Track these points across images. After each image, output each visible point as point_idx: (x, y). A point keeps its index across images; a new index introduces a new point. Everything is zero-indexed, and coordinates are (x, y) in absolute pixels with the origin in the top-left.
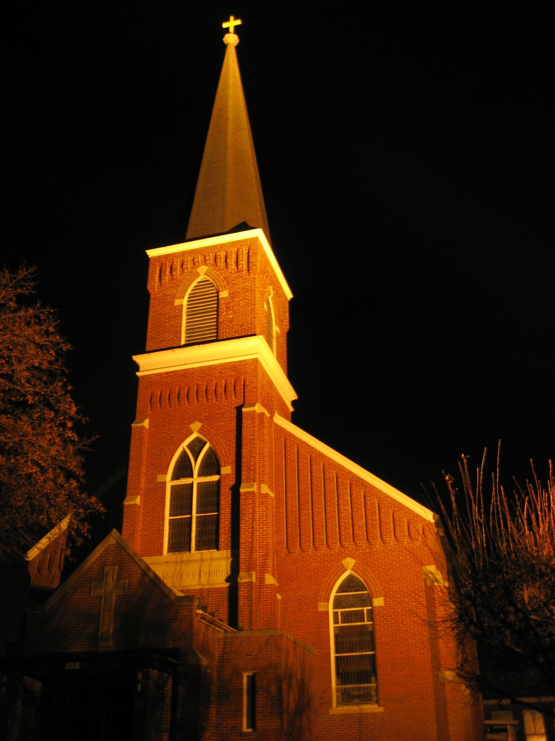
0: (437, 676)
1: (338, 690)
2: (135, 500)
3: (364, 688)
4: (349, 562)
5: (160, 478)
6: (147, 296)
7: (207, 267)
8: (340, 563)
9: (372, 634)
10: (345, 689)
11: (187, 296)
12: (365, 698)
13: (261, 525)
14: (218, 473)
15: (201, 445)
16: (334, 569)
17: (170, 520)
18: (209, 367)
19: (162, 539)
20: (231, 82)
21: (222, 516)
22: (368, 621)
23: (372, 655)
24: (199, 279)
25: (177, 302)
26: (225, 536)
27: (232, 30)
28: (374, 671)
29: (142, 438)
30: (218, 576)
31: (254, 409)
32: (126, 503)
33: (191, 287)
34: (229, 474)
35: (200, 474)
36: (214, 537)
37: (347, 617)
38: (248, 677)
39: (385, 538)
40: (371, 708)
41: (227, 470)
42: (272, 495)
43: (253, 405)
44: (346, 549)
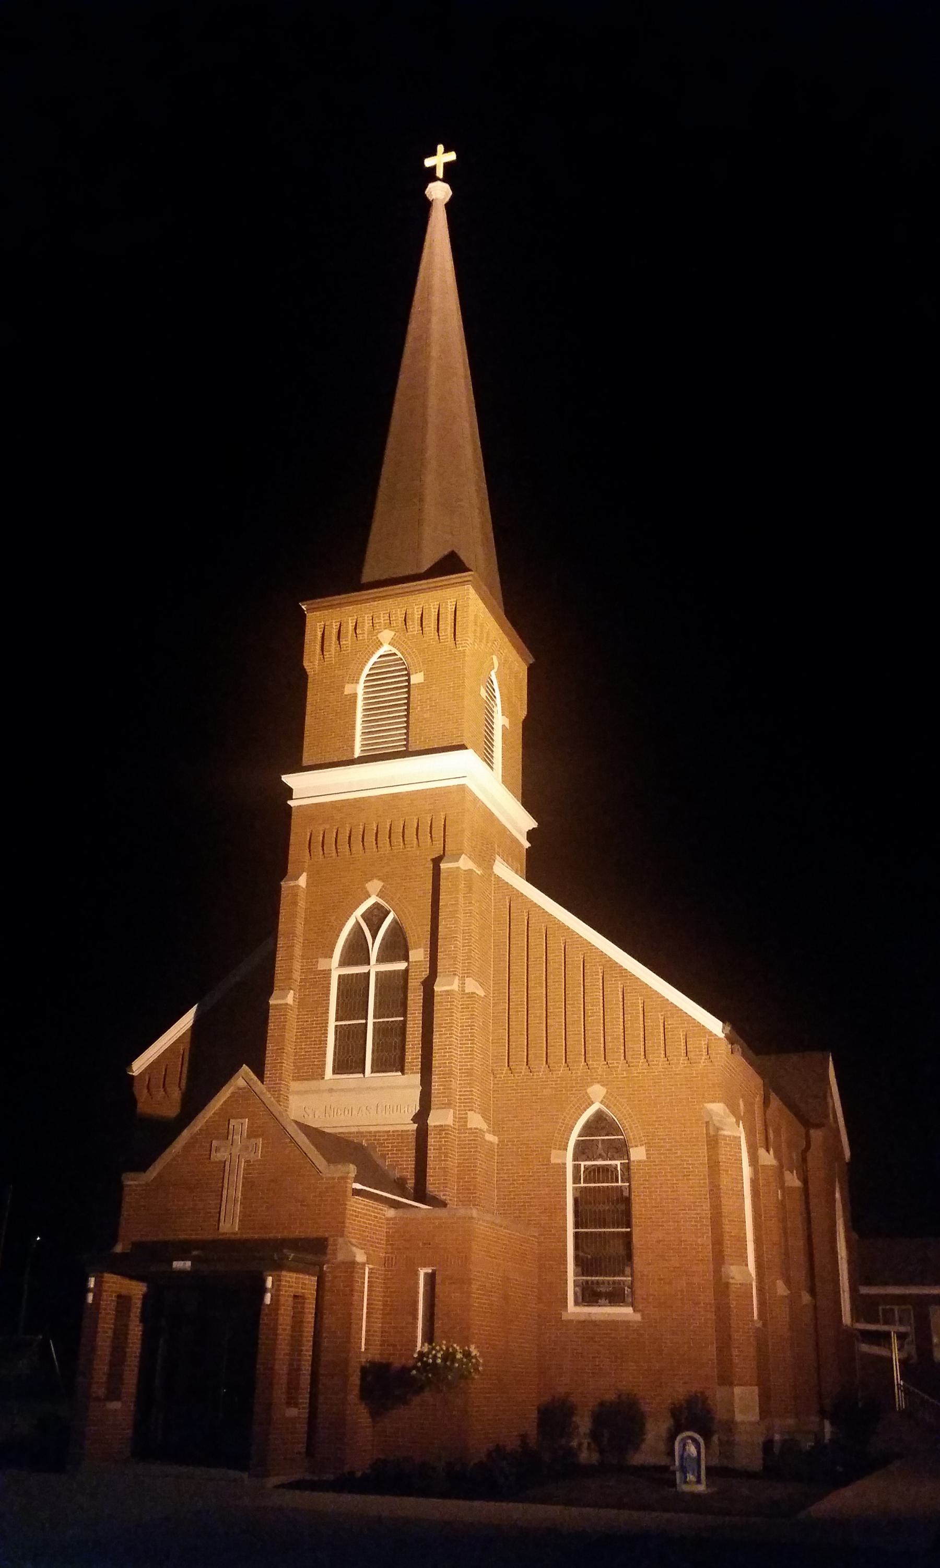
0: (717, 1271)
1: (576, 1284)
2: (286, 996)
3: (614, 1282)
4: (597, 1091)
5: (322, 965)
6: (303, 676)
7: (393, 633)
8: (584, 1092)
9: (628, 1201)
10: (587, 1282)
11: (363, 678)
12: (616, 1297)
13: (464, 1039)
14: (406, 958)
15: (382, 915)
16: (576, 1099)
17: (336, 1026)
18: (395, 796)
19: (324, 1055)
20: (436, 282)
21: (410, 1024)
22: (623, 1181)
23: (628, 1232)
24: (381, 652)
25: (348, 689)
26: (413, 1054)
27: (440, 173)
28: (629, 1257)
29: (295, 903)
30: (402, 1111)
31: (457, 866)
32: (272, 1002)
33: (370, 664)
34: (421, 961)
35: (381, 960)
36: (397, 1040)
37: (594, 1174)
38: (426, 1274)
39: (650, 1057)
40: (624, 1312)
41: (418, 955)
42: (481, 993)
43: (456, 858)
44: (593, 1071)
